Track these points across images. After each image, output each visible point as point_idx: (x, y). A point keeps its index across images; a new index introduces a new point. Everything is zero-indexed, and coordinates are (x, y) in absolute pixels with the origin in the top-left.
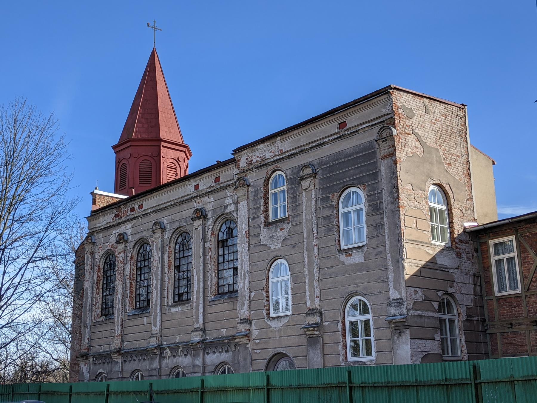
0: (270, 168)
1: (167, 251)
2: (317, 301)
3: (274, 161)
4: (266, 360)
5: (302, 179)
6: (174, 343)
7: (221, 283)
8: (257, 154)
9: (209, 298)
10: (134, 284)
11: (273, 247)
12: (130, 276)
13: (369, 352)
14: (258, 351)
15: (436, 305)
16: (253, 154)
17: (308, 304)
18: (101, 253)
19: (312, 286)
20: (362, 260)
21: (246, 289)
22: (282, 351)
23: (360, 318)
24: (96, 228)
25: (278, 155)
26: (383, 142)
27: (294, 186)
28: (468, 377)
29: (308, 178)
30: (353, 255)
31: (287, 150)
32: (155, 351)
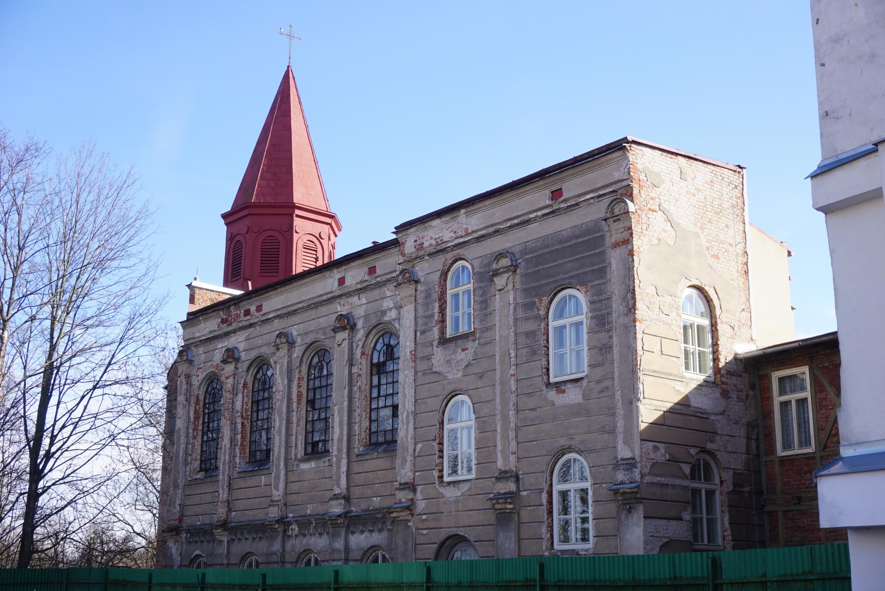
0: (450, 256)
2: (513, 459)
5: (496, 273)
6: (304, 516)
10: (248, 426)
11: (450, 376)
12: (242, 413)
14: (425, 532)
15: (687, 469)
16: (425, 233)
18: (201, 377)
19: (505, 437)
21: (409, 439)
24: (194, 338)
25: (462, 237)
26: (615, 221)
29: (504, 272)
30: (567, 391)
31: (475, 228)
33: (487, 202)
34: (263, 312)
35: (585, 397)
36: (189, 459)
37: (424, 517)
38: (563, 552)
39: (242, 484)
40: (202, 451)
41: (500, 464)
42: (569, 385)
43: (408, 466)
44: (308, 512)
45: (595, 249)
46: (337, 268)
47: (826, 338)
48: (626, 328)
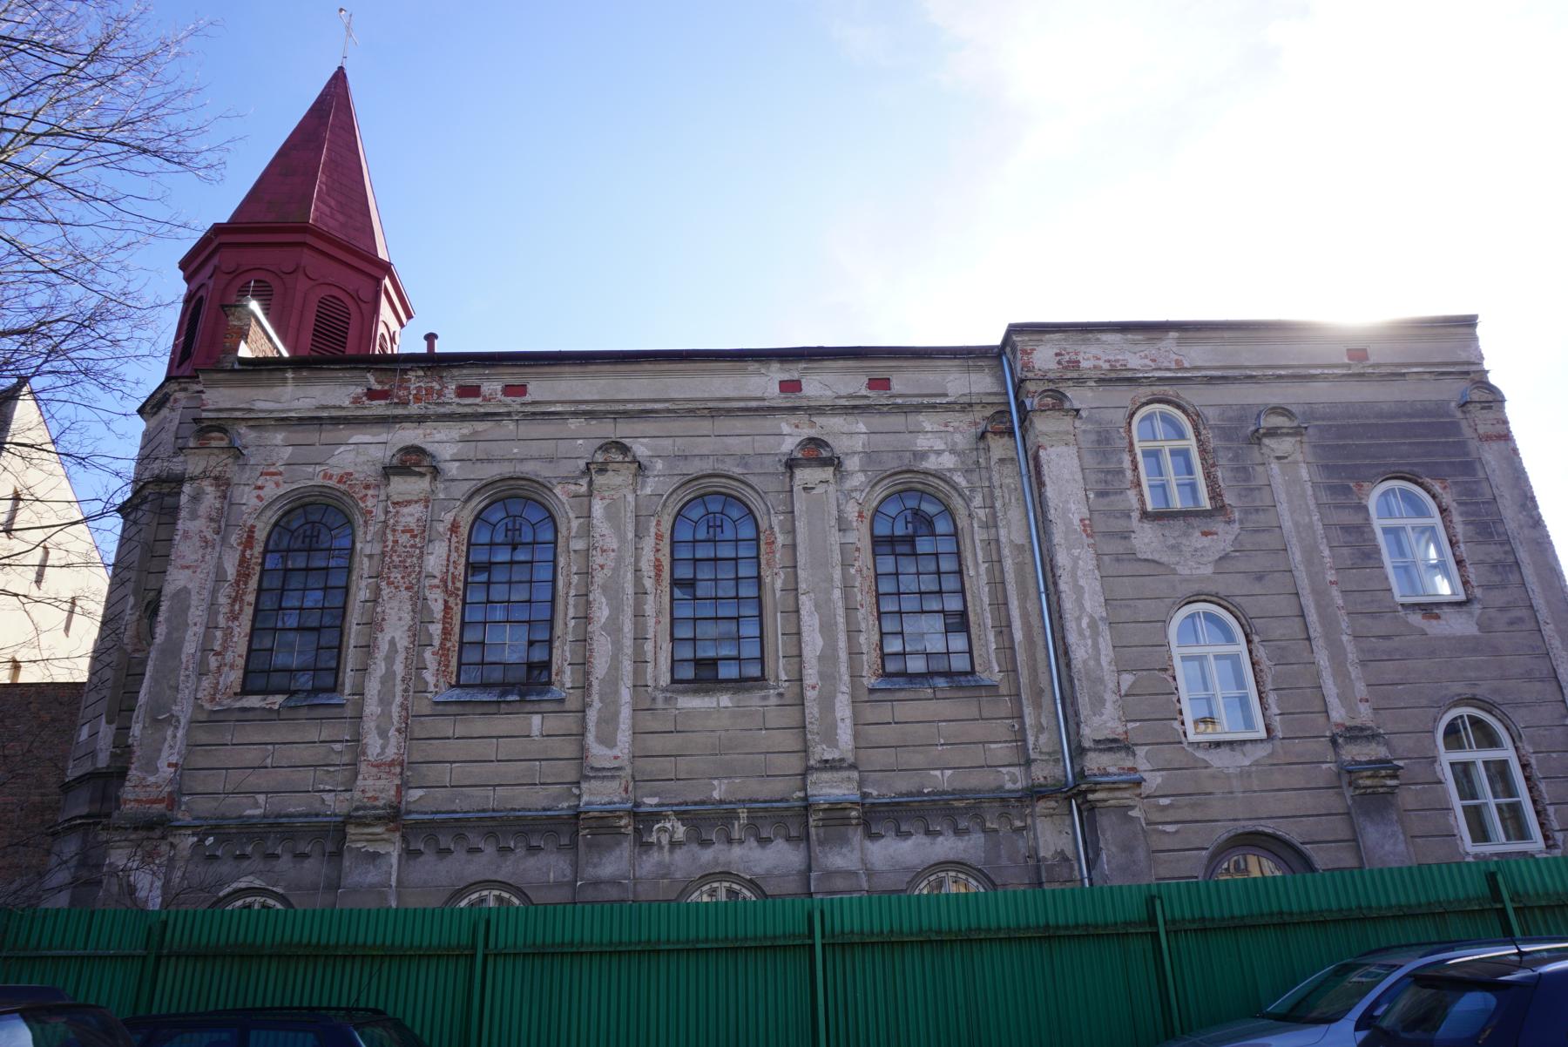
0: (1144, 392)
1: (653, 530)
3: (1160, 379)
6: (703, 803)
7: (894, 646)
8: (1094, 350)
9: (865, 681)
10: (457, 610)
11: (1183, 570)
12: (444, 581)
13: (1522, 833)
16: (1083, 348)
17: (1338, 714)
18: (271, 490)
21: (1104, 663)
23: (1478, 756)
24: (250, 410)
27: (1235, 445)
28: (490, 961)
29: (1288, 434)
31: (1199, 364)
32: (623, 823)
33: (841, 364)
34: (528, 398)
36: (213, 662)
37: (1164, 801)
39: (445, 727)
40: (250, 650)
41: (1338, 714)
42: (1446, 609)
44: (716, 795)
46: (782, 362)
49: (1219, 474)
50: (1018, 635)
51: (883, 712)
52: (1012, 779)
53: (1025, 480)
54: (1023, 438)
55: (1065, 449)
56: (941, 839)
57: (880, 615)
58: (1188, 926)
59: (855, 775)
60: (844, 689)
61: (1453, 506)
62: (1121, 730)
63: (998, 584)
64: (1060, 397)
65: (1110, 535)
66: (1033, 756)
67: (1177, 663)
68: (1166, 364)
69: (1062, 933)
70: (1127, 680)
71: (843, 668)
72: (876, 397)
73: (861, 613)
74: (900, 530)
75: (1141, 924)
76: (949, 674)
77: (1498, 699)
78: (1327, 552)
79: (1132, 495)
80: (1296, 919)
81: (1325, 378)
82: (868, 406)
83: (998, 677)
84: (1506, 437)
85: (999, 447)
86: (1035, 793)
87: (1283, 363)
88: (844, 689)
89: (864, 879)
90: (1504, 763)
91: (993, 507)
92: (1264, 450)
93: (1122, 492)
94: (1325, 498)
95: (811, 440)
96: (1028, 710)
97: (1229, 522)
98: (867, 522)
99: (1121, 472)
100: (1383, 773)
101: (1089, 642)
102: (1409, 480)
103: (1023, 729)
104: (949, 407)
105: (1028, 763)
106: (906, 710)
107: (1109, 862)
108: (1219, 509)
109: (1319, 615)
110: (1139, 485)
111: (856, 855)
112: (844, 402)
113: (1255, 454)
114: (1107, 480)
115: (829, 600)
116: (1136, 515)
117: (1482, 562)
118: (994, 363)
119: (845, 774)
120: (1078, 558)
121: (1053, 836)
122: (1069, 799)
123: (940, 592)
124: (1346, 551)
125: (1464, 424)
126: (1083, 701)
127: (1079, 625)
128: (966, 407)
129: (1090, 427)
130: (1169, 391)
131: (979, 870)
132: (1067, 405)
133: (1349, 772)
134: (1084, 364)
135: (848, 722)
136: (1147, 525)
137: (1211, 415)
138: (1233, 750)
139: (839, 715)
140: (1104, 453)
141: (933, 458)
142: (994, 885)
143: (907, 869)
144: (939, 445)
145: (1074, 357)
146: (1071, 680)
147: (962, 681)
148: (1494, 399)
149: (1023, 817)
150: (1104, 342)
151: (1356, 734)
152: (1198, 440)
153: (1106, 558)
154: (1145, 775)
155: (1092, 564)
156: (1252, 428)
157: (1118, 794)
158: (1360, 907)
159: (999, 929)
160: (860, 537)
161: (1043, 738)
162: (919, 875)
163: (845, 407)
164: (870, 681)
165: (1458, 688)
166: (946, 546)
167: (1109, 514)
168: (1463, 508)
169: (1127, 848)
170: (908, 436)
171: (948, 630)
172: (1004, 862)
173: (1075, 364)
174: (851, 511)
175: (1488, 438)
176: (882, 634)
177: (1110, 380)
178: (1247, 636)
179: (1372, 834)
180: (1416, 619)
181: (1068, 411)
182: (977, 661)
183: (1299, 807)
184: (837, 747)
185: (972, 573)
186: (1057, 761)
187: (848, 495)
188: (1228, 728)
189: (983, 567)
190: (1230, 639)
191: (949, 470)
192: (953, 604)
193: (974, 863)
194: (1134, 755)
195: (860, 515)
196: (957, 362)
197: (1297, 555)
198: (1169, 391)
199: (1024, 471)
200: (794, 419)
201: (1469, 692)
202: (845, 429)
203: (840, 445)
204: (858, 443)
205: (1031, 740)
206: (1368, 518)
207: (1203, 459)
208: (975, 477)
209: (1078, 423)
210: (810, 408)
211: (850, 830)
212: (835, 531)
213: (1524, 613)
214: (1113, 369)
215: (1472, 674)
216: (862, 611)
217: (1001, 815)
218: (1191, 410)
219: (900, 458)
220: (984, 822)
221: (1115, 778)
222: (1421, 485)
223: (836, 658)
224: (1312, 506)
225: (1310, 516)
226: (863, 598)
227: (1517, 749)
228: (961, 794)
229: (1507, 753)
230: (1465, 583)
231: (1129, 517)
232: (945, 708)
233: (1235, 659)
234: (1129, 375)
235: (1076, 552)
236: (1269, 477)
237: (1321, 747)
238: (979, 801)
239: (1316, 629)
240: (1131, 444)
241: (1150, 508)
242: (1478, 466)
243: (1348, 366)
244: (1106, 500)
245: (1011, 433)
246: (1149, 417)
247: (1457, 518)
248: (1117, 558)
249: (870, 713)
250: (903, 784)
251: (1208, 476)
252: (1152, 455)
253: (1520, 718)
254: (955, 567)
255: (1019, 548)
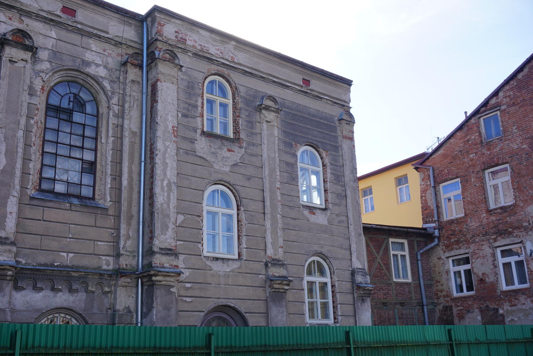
0: (214, 68)
3: (223, 64)
4: (202, 313)
7: (48, 173)
8: (195, 36)
11: (216, 167)
13: (325, 316)
14: (188, 299)
16: (189, 33)
17: (270, 252)
19: (274, 232)
20: (326, 223)
21: (171, 207)
22: (229, 304)
23: (317, 279)
25: (228, 60)
26: (347, 124)
27: (250, 109)
29: (273, 111)
30: (316, 214)
31: (242, 62)
35: (330, 222)
38: (312, 326)
42: (318, 211)
43: (170, 233)
45: (331, 132)
47: (386, 227)
48: (355, 189)
49: (240, 122)
50: (125, 183)
51: (37, 213)
52: (107, 264)
53: (144, 96)
54: (147, 72)
55: (171, 85)
56: (60, 294)
57: (43, 153)
58: (224, 350)
59: (14, 249)
60: (15, 194)
61: (328, 165)
62: (173, 244)
63: (118, 151)
64: (174, 56)
65: (185, 138)
66: (122, 252)
67: (205, 214)
68: (227, 57)
69: (163, 351)
70: (181, 218)
71: (17, 181)
72: (65, 18)
73: (33, 149)
74: (65, 104)
75: (202, 348)
76: (79, 197)
77: (329, 255)
78: (278, 173)
79: (199, 119)
80: (271, 349)
81: (89, 84)
82: (60, 23)
83: (108, 204)
84: (352, 139)
85: (133, 73)
86: (119, 273)
87: (277, 75)
88: (15, 194)
89: (9, 314)
90: (326, 284)
91: (123, 106)
92: (262, 116)
93: (195, 117)
94: (282, 147)
95: (20, 31)
96: (123, 226)
97: (240, 147)
98: (46, 93)
99: (196, 107)
100: (285, 282)
101: (166, 194)
102: (314, 148)
103: (118, 236)
104: (108, 40)
105: (118, 255)
106: (52, 214)
107: (156, 315)
108: (237, 140)
109: (271, 203)
110: (203, 116)
111: (6, 299)
112: (44, 14)
113: (257, 117)
114: (188, 110)
115: (14, 136)
116: (199, 132)
117: (334, 193)
118: (138, 24)
119: (8, 247)
120: (168, 147)
121: (125, 298)
122: (137, 279)
123: (82, 148)
124: (285, 174)
125: (338, 128)
126: (158, 225)
127: (162, 184)
128: (118, 44)
129: (185, 77)
130: (226, 71)
131: (80, 315)
132: (177, 62)
133: (271, 280)
134: (188, 42)
135: (14, 215)
136: (203, 139)
137: (242, 89)
138: (223, 263)
139: (9, 210)
140: (190, 94)
141: (93, 67)
142: (87, 323)
143: (37, 310)
144: (98, 61)
145: (184, 37)
146: (152, 214)
147: (88, 203)
148: (351, 121)
149: (110, 286)
150: (200, 34)
151: (276, 262)
152: (234, 102)
153: (181, 151)
154: (182, 270)
155: (174, 152)
156: (258, 103)
157: (168, 279)
158: (297, 344)
159: (129, 348)
160: (40, 101)
161: (129, 243)
162: (43, 314)
163: (46, 18)
164: (32, 192)
165: (316, 248)
166: (90, 121)
167: (187, 127)
168: (332, 166)
169: (167, 308)
170: (81, 49)
171: (83, 171)
172: (95, 311)
173: (184, 41)
174: (38, 84)
175: (345, 137)
176: (42, 165)
177: (200, 56)
178: (238, 206)
179: (274, 311)
180: (306, 212)
181: (177, 65)
182: (97, 193)
183: (246, 297)
184: (4, 230)
185: (103, 141)
186: (134, 256)
187: (37, 73)
188: (221, 252)
189: (111, 139)
190: (228, 205)
191: (102, 77)
192: (88, 156)
193: (77, 310)
194: (178, 259)
195: (43, 89)
196: (117, 16)
197: (267, 172)
198: (226, 71)
199: (144, 91)
200: (9, 14)
201: (320, 250)
202: (42, 32)
203: (39, 41)
204: (50, 43)
205: (122, 243)
206: (296, 161)
207: (234, 112)
208: (116, 86)
209: (180, 73)
210: (22, 10)
211: (5, 282)
212: (26, 94)
213: (344, 218)
214: (202, 51)
215: (322, 242)
216: (34, 148)
217: (98, 284)
218: (233, 85)
219: (74, 61)
220: (87, 287)
221: (167, 270)
222: (318, 151)
223: (13, 174)
224: (277, 150)
225: (275, 154)
226: (36, 140)
227: (331, 278)
228: (77, 268)
229: (327, 280)
230: (326, 201)
231: (196, 132)
232: (75, 217)
233: (230, 216)
234: (209, 56)
235: (167, 143)
236: (261, 130)
237: (260, 267)
238: (87, 274)
239: (268, 210)
240: (203, 94)
241: (205, 130)
242: (340, 149)
243: (302, 87)
244: (186, 120)
245: (141, 67)
246: (212, 82)
247: (329, 171)
248: (186, 153)
249: (29, 212)
250: (42, 259)
251: (235, 121)
252: (210, 102)
253: (335, 264)
254: (94, 135)
255: (134, 133)
